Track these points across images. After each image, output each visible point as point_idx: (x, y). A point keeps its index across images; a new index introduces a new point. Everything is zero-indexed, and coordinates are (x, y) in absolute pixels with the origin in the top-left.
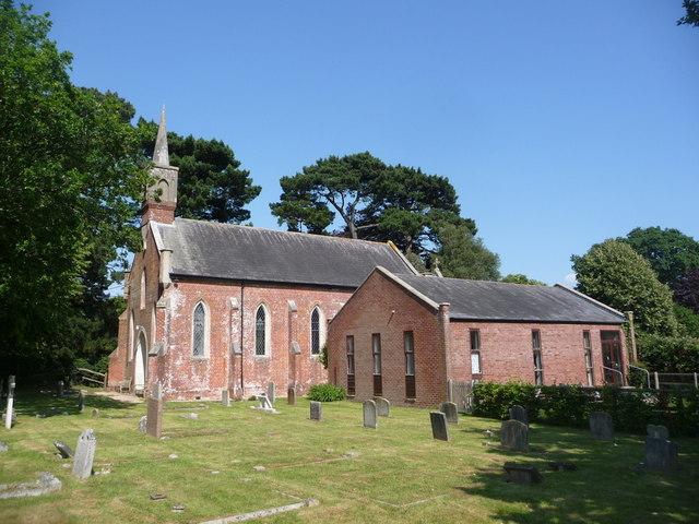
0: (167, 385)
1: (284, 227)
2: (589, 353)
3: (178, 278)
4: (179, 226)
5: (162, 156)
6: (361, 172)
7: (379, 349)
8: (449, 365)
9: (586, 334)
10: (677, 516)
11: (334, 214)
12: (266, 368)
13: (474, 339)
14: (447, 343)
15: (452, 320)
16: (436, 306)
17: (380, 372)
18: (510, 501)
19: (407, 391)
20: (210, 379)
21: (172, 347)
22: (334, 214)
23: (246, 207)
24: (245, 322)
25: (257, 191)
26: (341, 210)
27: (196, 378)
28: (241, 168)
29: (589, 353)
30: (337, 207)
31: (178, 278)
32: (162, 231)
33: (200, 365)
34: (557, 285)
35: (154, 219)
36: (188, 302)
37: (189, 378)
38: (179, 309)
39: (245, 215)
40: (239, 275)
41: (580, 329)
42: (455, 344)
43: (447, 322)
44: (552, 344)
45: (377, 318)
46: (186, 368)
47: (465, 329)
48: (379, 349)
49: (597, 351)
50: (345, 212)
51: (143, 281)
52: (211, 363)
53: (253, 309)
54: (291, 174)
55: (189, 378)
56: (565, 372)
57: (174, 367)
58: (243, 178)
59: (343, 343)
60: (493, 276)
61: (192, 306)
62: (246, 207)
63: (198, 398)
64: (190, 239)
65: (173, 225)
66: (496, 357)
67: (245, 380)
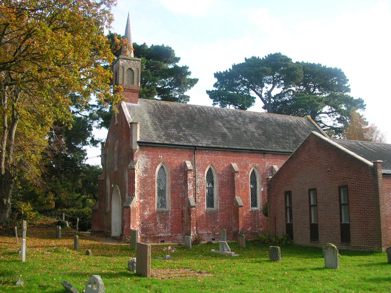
1: (218, 106)
3: (142, 144)
4: (141, 104)
7: (316, 200)
8: (382, 214)
10: (333, 245)
11: (254, 98)
12: (215, 218)
15: (384, 174)
16: (371, 164)
18: (134, 188)
19: (317, 228)
20: (171, 226)
21: (141, 201)
22: (254, 98)
23: (186, 94)
24: (198, 181)
25: (194, 82)
26: (260, 96)
28: (180, 64)
30: (257, 93)
32: (129, 108)
37: (155, 225)
38: (146, 171)
39: (187, 98)
40: (192, 142)
43: (380, 178)
48: (316, 200)
50: (263, 96)
51: (6, 138)
52: (172, 214)
54: (223, 70)
55: (155, 225)
59: (281, 197)
61: (156, 168)
62: (186, 94)
63: (163, 242)
64: (152, 114)
65: (138, 105)
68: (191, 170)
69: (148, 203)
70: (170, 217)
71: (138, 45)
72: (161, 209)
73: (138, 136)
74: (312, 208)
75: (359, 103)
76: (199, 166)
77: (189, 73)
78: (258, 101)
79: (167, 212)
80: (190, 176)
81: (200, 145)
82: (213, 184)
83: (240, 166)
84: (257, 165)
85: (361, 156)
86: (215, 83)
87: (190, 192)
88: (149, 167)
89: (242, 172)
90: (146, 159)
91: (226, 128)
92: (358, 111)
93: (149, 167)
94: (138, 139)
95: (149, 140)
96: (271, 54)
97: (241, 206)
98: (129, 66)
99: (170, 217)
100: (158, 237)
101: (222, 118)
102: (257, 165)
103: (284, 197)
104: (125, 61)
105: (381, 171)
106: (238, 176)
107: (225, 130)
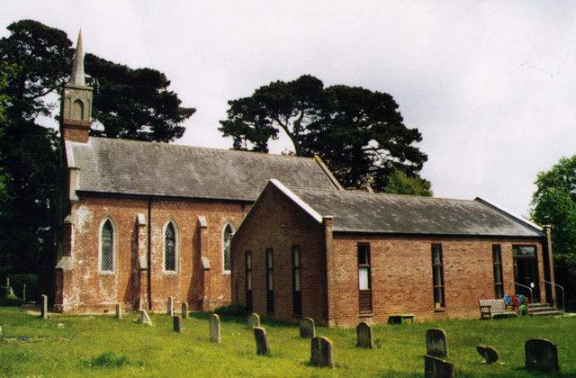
0: (74, 299)
2: (498, 269)
5: (81, 77)
6: (306, 91)
8: (331, 281)
9: (497, 251)
11: (277, 131)
13: (364, 257)
14: (330, 258)
15: (336, 234)
16: (319, 218)
17: (370, 285)
21: (80, 262)
23: (181, 124)
26: (285, 128)
27: (104, 292)
28: (169, 89)
29: (498, 269)
31: (86, 196)
32: (75, 149)
33: (108, 280)
34: (478, 199)
35: (70, 139)
36: (95, 217)
38: (87, 225)
41: (488, 245)
42: (339, 259)
43: (330, 240)
44: (455, 258)
45: (275, 236)
46: (94, 281)
47: (353, 246)
49: (508, 265)
53: (161, 226)
56: (469, 288)
57: (82, 281)
58: (172, 100)
60: (428, 194)
61: (99, 222)
62: (181, 124)
66: (389, 273)
67: (152, 295)
68: (143, 225)
69: (89, 265)
70: (117, 282)
71: (131, 70)
72: (105, 272)
73: (76, 183)
74: (297, 271)
75: (415, 135)
76: (155, 218)
77: (180, 102)
78: (282, 134)
79: (113, 276)
80: (143, 232)
81: (156, 194)
82: (174, 242)
83: (209, 220)
84: (233, 218)
85: (315, 209)
86: (191, 117)
87: (142, 252)
88: (91, 222)
89: (212, 228)
90: (87, 212)
91: (198, 172)
92: (414, 144)
93: (91, 222)
94: (78, 188)
95: (91, 189)
96: (176, 95)
97: (208, 269)
98: (77, 97)
99: (117, 282)
100: (101, 306)
101: (196, 160)
102: (233, 218)
103: (290, 253)
104: (73, 91)
105: (330, 229)
106: (205, 233)
107: (196, 176)
